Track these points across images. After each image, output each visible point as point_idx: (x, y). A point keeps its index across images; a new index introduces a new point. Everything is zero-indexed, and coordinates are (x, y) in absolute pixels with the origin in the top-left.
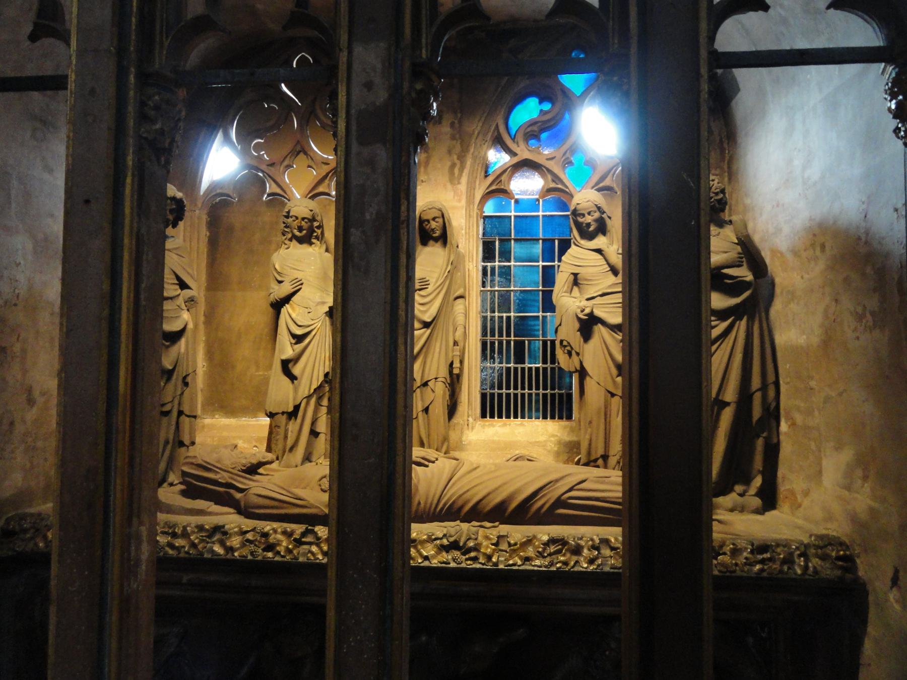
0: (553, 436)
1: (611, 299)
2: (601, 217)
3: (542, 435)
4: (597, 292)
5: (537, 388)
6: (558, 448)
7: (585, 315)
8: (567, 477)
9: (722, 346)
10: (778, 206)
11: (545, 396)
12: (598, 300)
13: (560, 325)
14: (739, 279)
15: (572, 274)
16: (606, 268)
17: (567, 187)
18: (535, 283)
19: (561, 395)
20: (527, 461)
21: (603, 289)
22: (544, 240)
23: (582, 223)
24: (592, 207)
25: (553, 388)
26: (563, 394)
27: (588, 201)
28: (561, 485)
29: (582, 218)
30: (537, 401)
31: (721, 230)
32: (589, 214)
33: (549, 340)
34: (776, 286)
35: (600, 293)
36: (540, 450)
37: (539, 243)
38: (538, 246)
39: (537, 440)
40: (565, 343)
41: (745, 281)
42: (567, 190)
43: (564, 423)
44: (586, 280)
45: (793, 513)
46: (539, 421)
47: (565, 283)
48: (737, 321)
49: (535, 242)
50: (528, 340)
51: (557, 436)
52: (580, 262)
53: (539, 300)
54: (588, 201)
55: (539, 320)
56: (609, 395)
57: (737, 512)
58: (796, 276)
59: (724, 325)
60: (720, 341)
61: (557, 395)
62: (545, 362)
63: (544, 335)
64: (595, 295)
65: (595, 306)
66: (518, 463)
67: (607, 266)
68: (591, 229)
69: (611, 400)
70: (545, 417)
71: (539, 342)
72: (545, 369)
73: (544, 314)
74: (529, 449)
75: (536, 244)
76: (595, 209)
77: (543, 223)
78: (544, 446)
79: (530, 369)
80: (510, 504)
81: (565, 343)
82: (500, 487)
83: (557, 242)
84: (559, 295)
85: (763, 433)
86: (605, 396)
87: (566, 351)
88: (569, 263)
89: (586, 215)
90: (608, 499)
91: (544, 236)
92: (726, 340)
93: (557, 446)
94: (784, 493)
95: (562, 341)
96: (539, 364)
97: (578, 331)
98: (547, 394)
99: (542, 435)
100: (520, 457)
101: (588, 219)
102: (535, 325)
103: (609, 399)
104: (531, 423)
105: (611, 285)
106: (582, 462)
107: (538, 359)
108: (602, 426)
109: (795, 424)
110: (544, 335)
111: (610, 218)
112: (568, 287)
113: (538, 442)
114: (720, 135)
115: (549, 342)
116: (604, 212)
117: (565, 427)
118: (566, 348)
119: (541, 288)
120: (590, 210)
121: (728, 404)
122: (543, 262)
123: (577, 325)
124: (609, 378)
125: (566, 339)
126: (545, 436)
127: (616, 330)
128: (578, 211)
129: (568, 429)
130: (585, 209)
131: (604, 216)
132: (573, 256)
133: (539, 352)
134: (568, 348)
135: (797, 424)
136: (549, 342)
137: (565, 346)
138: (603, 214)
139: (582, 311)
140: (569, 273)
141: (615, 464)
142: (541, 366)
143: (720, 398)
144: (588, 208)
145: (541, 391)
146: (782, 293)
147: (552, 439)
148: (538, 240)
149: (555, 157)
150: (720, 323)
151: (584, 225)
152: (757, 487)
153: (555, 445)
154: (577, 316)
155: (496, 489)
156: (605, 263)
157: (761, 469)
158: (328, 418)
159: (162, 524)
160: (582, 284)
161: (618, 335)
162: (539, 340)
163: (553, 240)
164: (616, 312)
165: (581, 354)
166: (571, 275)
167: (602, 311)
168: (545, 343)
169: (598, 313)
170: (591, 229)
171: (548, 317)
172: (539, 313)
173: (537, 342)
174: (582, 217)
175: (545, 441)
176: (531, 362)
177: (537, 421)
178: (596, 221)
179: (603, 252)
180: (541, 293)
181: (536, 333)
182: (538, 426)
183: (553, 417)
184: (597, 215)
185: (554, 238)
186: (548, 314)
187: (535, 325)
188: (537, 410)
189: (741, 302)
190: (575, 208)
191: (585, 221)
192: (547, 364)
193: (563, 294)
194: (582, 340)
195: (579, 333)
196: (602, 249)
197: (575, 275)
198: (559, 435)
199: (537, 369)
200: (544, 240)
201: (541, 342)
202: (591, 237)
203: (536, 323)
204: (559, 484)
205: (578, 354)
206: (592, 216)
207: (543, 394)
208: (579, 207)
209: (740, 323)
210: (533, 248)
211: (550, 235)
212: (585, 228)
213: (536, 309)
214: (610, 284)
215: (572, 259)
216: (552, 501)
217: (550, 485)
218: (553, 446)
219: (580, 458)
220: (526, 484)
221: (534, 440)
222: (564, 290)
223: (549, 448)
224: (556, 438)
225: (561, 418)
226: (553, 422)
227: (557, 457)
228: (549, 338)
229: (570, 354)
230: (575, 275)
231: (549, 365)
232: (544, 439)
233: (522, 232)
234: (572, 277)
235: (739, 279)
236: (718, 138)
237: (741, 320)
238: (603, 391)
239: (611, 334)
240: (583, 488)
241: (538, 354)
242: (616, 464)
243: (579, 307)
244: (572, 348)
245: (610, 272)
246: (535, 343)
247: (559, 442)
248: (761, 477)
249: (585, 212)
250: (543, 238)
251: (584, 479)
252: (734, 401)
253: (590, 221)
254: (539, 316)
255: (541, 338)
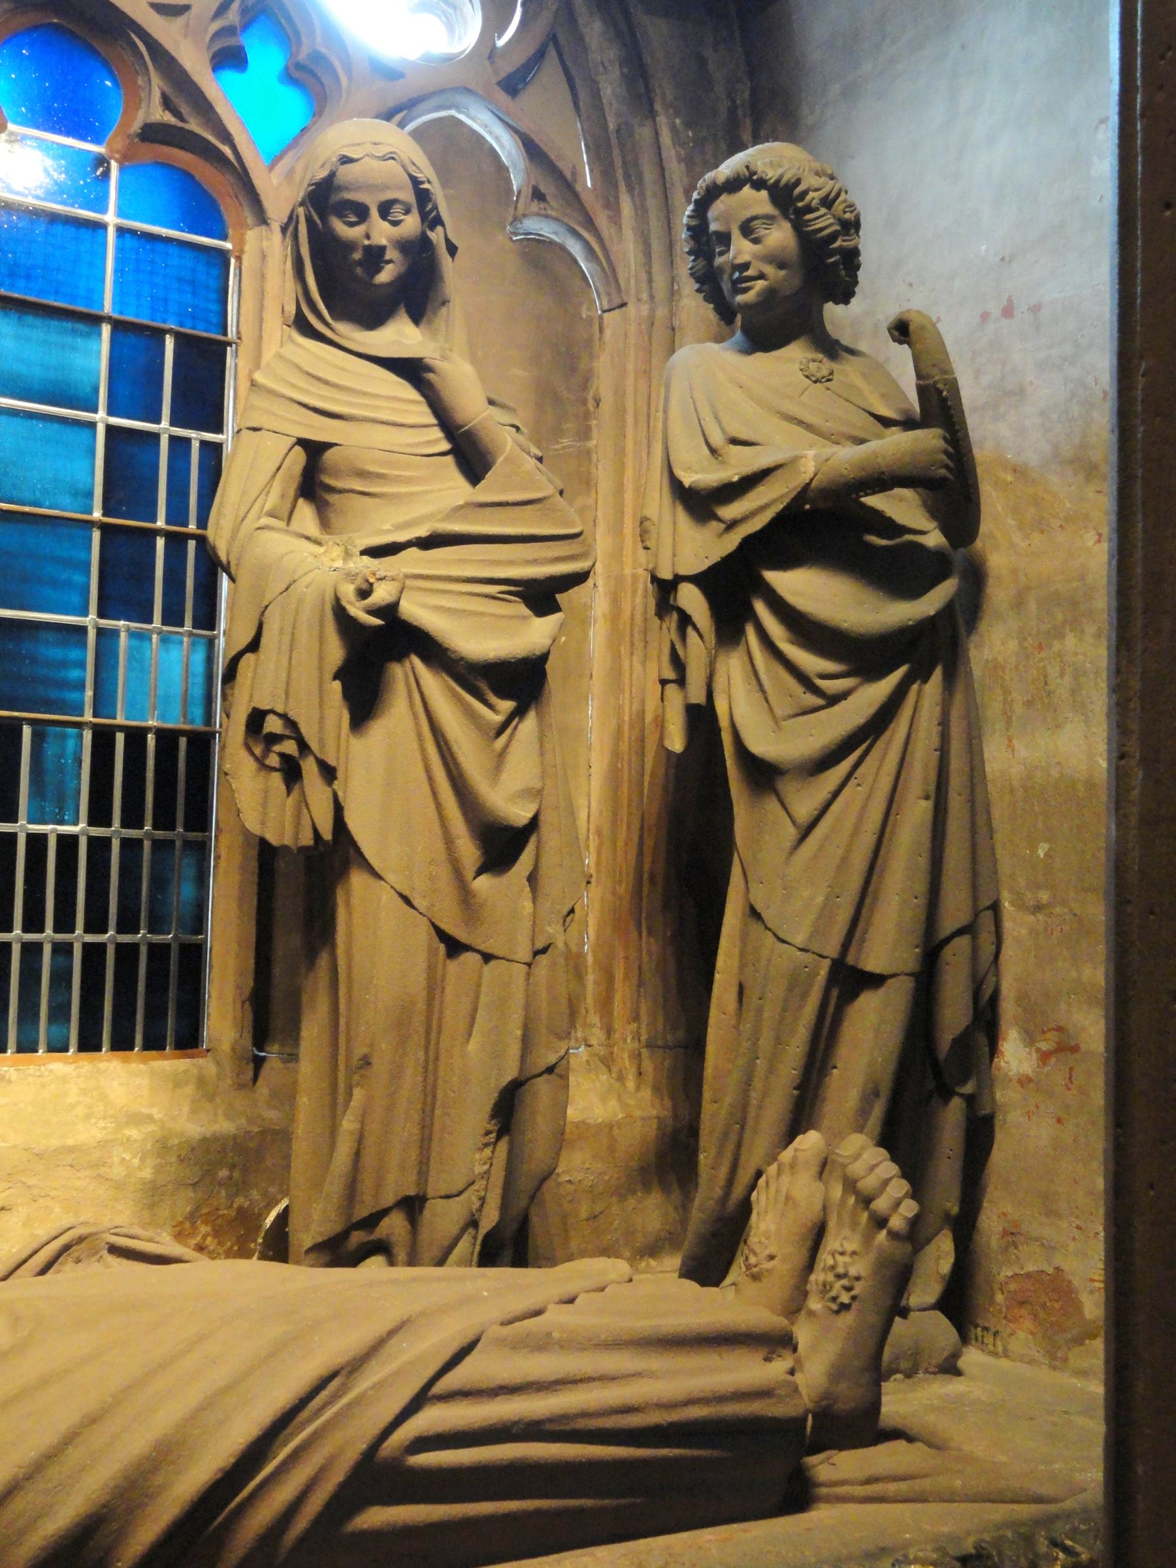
0: (136, 1119)
1: (448, 562)
2: (424, 234)
3: (88, 1117)
4: (408, 525)
5: (64, 923)
6: (158, 1169)
7: (373, 612)
8: (394, 1341)
9: (861, 770)
10: (1008, 312)
11: (93, 953)
12: (411, 561)
13: (254, 646)
14: (909, 537)
15: (301, 442)
16: (436, 441)
17: (227, 138)
18: (75, 494)
19: (158, 952)
20: (111, 1260)
21: (429, 517)
22: (120, 327)
23: (350, 246)
24: (400, 188)
25: (127, 924)
26: (166, 947)
27: (384, 158)
28: (373, 1387)
29: (352, 225)
30: (61, 978)
31: (835, 366)
32: (385, 210)
33: (121, 728)
34: (991, 582)
35: (422, 532)
36: (78, 1183)
37: (100, 335)
38: (92, 344)
39: (70, 1142)
40: (273, 725)
41: (920, 547)
42: (226, 150)
43: (169, 1064)
44: (363, 474)
45: (1053, 1357)
46: (66, 1062)
47: (274, 476)
48: (913, 683)
49: (80, 326)
50: (32, 722)
51: (150, 1118)
52: (333, 400)
53: (88, 565)
54: (384, 158)
55: (84, 645)
56: (442, 948)
57: (899, 1376)
58: (1090, 543)
59: (881, 689)
60: (864, 746)
61: (144, 950)
62: (99, 814)
63: (102, 703)
64: (402, 537)
65: (409, 582)
66: (67, 1274)
67: (437, 433)
68: (385, 276)
69: (444, 965)
70: (89, 1044)
71: (80, 737)
72: (99, 847)
73: (104, 623)
74: (33, 1181)
75: (88, 335)
76: (408, 196)
77: (117, 259)
78: (95, 1165)
79: (37, 843)
80: (122, 1534)
81: (273, 725)
82: (69, 1440)
83: (170, 343)
84: (250, 523)
85: (964, 1082)
86: (432, 952)
87: (273, 760)
88: (283, 396)
89: (374, 213)
90: (582, 1424)
91: (121, 313)
92: (880, 744)
93: (151, 1162)
94: (1013, 1286)
95: (256, 719)
96: (76, 823)
97: (335, 678)
98: (102, 947)
99: (88, 1117)
100: (81, 1240)
101: (381, 232)
102: (64, 664)
103: (440, 966)
104: (32, 1069)
105: (461, 507)
106: (304, 1236)
107: (70, 805)
108: (411, 1078)
109: (1075, 1049)
110: (102, 703)
111: (452, 249)
112: (283, 496)
113: (71, 1150)
114: (730, 96)
115: (120, 737)
116: (437, 221)
117: (177, 1083)
118: (277, 748)
119: (97, 515)
120: (389, 195)
121: (876, 981)
122: (110, 413)
123: (336, 653)
124: (444, 874)
125: (280, 710)
126: (102, 1124)
127: (483, 686)
128: (340, 188)
129: (190, 1089)
130: (370, 188)
131: (436, 236)
132: (309, 374)
133: (79, 776)
134: (290, 747)
135: (1083, 1047)
136: (120, 737)
137: (273, 739)
138: (432, 228)
139: (364, 593)
140: (294, 440)
141: (455, 1230)
142: (83, 832)
143: (850, 960)
144: (384, 187)
145: (79, 936)
146: (1019, 603)
147: (134, 1133)
148: (95, 320)
149: (186, 8)
150: (861, 684)
151: (357, 256)
152: (943, 1277)
153: (142, 1159)
154: (340, 613)
155: (51, 1456)
156: (432, 420)
157: (955, 1210)
158: (877, 457)
159: (729, 270)
160: (341, 491)
161: (490, 706)
162: (79, 725)
163: (158, 334)
164: (482, 614)
165: (340, 774)
166: (298, 448)
167: (425, 606)
168: (103, 738)
169: (414, 610)
170: (385, 276)
171: (123, 635)
172: (86, 615)
173: (72, 731)
174: (353, 219)
175: (103, 1144)
176: (43, 812)
177: (59, 1060)
178: (404, 246)
179: (431, 376)
180: (96, 535)
181: (73, 696)
182: (64, 1079)
183: (122, 1043)
184: (411, 224)
185: (162, 325)
186: (122, 622)
187: (64, 664)
188: (59, 1013)
189: (940, 614)
190: (332, 175)
191: (368, 237)
192: (109, 825)
193: (265, 521)
194: (346, 716)
195: (337, 685)
196: (428, 361)
197: (314, 450)
198: (157, 1113)
199: (67, 844)
200: (120, 327)
201: (88, 735)
202: (373, 319)
203: (74, 654)
204: (363, 1383)
205: (329, 773)
206: (395, 223)
207: (86, 947)
208: (346, 173)
209: (920, 691)
210: (74, 349)
211: (146, 311)
212: (359, 271)
213: (76, 599)
214: (461, 502)
215: (303, 383)
216: (337, 1476)
217: (324, 1395)
218: (136, 1161)
219: (286, 1209)
220: (209, 1404)
221: (54, 1143)
222: (268, 507)
223: (118, 1172)
224: (150, 1128)
225: (154, 1043)
226: (125, 1061)
227: (152, 1206)
228: (120, 720)
229: (291, 772)
230: (314, 450)
231: (115, 831)
232: (99, 1135)
233: (28, 277)
234: (299, 457)
235: (909, 537)
236: (723, 106)
237: (925, 679)
238: (423, 935)
239: (459, 699)
240: (468, 1387)
241: (72, 785)
242: (463, 1231)
243: (351, 576)
244: (303, 746)
245: (450, 459)
246: (64, 737)
247: (162, 1146)
248: (950, 1235)
249: (372, 202)
250: (116, 316)
251: (466, 1341)
252: (908, 971)
253: (384, 242)
254: (82, 630)
255: (88, 717)
